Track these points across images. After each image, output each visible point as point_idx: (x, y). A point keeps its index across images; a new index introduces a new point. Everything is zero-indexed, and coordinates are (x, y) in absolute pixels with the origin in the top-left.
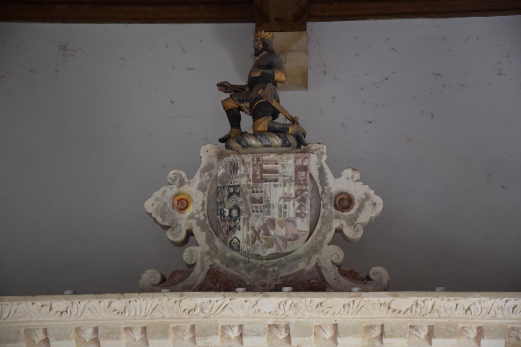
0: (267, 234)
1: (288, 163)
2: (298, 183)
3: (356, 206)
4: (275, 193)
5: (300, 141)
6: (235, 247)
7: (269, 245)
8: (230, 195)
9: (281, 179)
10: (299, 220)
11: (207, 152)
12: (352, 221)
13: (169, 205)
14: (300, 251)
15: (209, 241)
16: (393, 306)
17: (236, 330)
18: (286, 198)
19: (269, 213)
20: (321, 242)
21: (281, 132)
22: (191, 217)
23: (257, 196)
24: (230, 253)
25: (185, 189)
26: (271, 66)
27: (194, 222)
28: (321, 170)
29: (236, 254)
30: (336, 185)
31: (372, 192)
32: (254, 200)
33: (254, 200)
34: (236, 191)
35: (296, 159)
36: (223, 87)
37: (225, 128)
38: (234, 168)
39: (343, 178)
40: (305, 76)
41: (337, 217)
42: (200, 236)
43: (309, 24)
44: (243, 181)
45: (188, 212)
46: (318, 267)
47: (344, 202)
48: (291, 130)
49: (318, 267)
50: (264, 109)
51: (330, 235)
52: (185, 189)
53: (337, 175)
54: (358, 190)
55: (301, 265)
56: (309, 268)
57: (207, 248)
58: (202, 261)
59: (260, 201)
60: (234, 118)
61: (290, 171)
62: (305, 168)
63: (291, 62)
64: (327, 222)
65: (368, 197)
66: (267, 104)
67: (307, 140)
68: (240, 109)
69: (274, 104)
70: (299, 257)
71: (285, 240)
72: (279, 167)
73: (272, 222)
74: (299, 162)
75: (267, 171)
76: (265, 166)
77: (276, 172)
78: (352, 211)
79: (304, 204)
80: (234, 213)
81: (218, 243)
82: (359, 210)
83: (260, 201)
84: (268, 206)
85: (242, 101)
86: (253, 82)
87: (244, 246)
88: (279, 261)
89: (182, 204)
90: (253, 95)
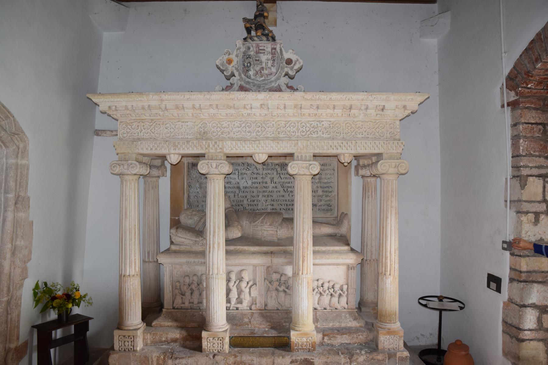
0: (261, 72)
1: (268, 46)
2: (272, 54)
3: (293, 63)
4: (264, 58)
5: (274, 39)
6: (249, 77)
7: (262, 77)
8: (247, 58)
9: (266, 52)
10: (272, 68)
11: (239, 43)
12: (292, 69)
13: (225, 62)
14: (273, 79)
15: (240, 75)
16: (305, 97)
17: (249, 106)
18: (268, 60)
19: (261, 65)
20: (280, 76)
21: (267, 35)
22: (233, 67)
23: (257, 59)
24: (247, 80)
25: (231, 56)
26: (262, 11)
27: (234, 68)
28: (281, 50)
29: (249, 80)
30: (286, 56)
31: (299, 58)
32: (256, 60)
33: (256, 60)
34: (249, 57)
35: (272, 45)
36: (245, 20)
37: (245, 34)
38: (249, 48)
39: (289, 53)
40: (276, 21)
41: (286, 67)
42: (236, 74)
43: (277, 2)
44: (252, 53)
45: (232, 65)
46: (279, 85)
47: (289, 62)
48: (270, 35)
49: (279, 85)
50: (260, 27)
51: (284, 74)
52: (231, 56)
53: (287, 52)
54: (294, 57)
55: (273, 84)
56: (276, 85)
57: (239, 78)
58: (237, 82)
59: (258, 60)
60: (249, 30)
61: (269, 49)
62: (275, 49)
63: (271, 16)
64: (282, 68)
65: (298, 60)
66: (261, 25)
67: (276, 38)
68: (251, 27)
69: (264, 25)
70: (272, 81)
71: (267, 75)
72: (265, 48)
73: (263, 68)
74: (273, 46)
75: (261, 50)
76: (260, 48)
77: (264, 50)
78: (292, 65)
79: (87, 298)
80: (249, 64)
81: (243, 76)
82: (294, 65)
83: (258, 60)
84: (261, 62)
85: (252, 24)
86: (256, 17)
87: (252, 77)
88: (280, 333)
89: (230, 61)
90: (256, 21)
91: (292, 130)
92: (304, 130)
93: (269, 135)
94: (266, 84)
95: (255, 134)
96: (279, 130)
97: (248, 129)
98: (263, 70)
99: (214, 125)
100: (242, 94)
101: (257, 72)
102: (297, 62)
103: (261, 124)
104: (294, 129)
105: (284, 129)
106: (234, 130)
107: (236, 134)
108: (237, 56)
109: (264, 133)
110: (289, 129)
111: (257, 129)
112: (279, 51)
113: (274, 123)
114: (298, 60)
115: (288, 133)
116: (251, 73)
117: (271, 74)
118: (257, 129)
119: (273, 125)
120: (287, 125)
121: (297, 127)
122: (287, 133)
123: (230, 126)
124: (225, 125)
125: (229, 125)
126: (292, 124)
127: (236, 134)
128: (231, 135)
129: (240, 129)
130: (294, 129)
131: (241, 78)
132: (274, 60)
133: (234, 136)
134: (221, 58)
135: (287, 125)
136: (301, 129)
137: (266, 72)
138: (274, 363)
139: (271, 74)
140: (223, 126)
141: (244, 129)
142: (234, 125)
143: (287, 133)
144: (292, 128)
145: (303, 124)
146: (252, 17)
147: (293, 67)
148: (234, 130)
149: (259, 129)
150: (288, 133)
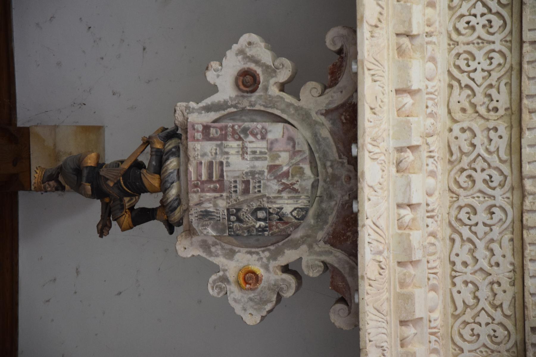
0: (286, 175)
2: (224, 138)
3: (253, 66)
4: (237, 165)
7: (301, 172)
8: (239, 220)
9: (219, 158)
10: (270, 136)
11: (186, 248)
12: (271, 71)
13: (252, 295)
15: (295, 245)
16: (374, 22)
17: (403, 212)
18: (243, 151)
19: (261, 173)
20: (297, 109)
21: (161, 159)
22: (266, 267)
25: (231, 275)
26: (78, 171)
27: (273, 264)
28: (208, 109)
29: (311, 213)
30: (226, 91)
31: (235, 47)
32: (246, 191)
33: (246, 191)
34: (234, 213)
35: (194, 139)
36: (103, 229)
37: (156, 227)
38: (206, 215)
39: (218, 82)
41: (266, 89)
42: (289, 256)
43: (19, 124)
44: (222, 204)
45: (260, 271)
46: (327, 113)
49: (327, 113)
50: (133, 178)
51: (288, 98)
52: (231, 275)
54: (233, 64)
55: (325, 133)
56: (328, 124)
57: (304, 247)
58: (320, 254)
59: (247, 183)
61: (209, 147)
62: (206, 128)
64: (271, 101)
65: (241, 52)
66: (126, 175)
67: (170, 126)
69: (126, 166)
70: (315, 135)
71: (295, 153)
72: (205, 161)
73: (272, 168)
74: (199, 135)
75: (210, 175)
76: (204, 178)
78: (259, 71)
80: (261, 214)
81: (298, 234)
82: (257, 62)
83: (247, 183)
84: (252, 173)
85: (122, 207)
86: (98, 193)
87: (302, 202)
89: (250, 278)
91: (485, 64)
92: (483, 21)
93: (503, 144)
94: (325, 155)
95: (498, 192)
96: (482, 110)
97: (482, 216)
98: (279, 166)
99: (467, 332)
100: (367, 236)
101: (286, 187)
102: (249, 53)
103: (463, 170)
104: (480, 55)
105: (479, 91)
106: (484, 263)
107: (497, 258)
108: (231, 255)
109: (494, 160)
110: (478, 76)
111: (480, 185)
112: (213, 116)
113: (456, 128)
114: (241, 52)
115: (495, 75)
116: (288, 206)
117: (291, 139)
118: (480, 185)
119: (463, 130)
120: (465, 80)
121: (470, 48)
122: (493, 80)
123: (469, 277)
124: (467, 295)
125: (466, 283)
126: (462, 63)
127: (497, 258)
128: (503, 273)
129: (481, 245)
130: (480, 55)
131: (304, 240)
132: (245, 131)
133: (506, 266)
134: (238, 310)
135: (465, 80)
136: (480, 31)
137: (284, 159)
138: (533, 78)
139: (291, 139)
140: (471, 301)
141: (481, 229)
142: (465, 264)
143: (493, 80)
144: (473, 65)
145: (461, 25)
146: (97, 205)
147: (266, 67)
148: (484, 263)
149: (479, 177)
150: (495, 75)
